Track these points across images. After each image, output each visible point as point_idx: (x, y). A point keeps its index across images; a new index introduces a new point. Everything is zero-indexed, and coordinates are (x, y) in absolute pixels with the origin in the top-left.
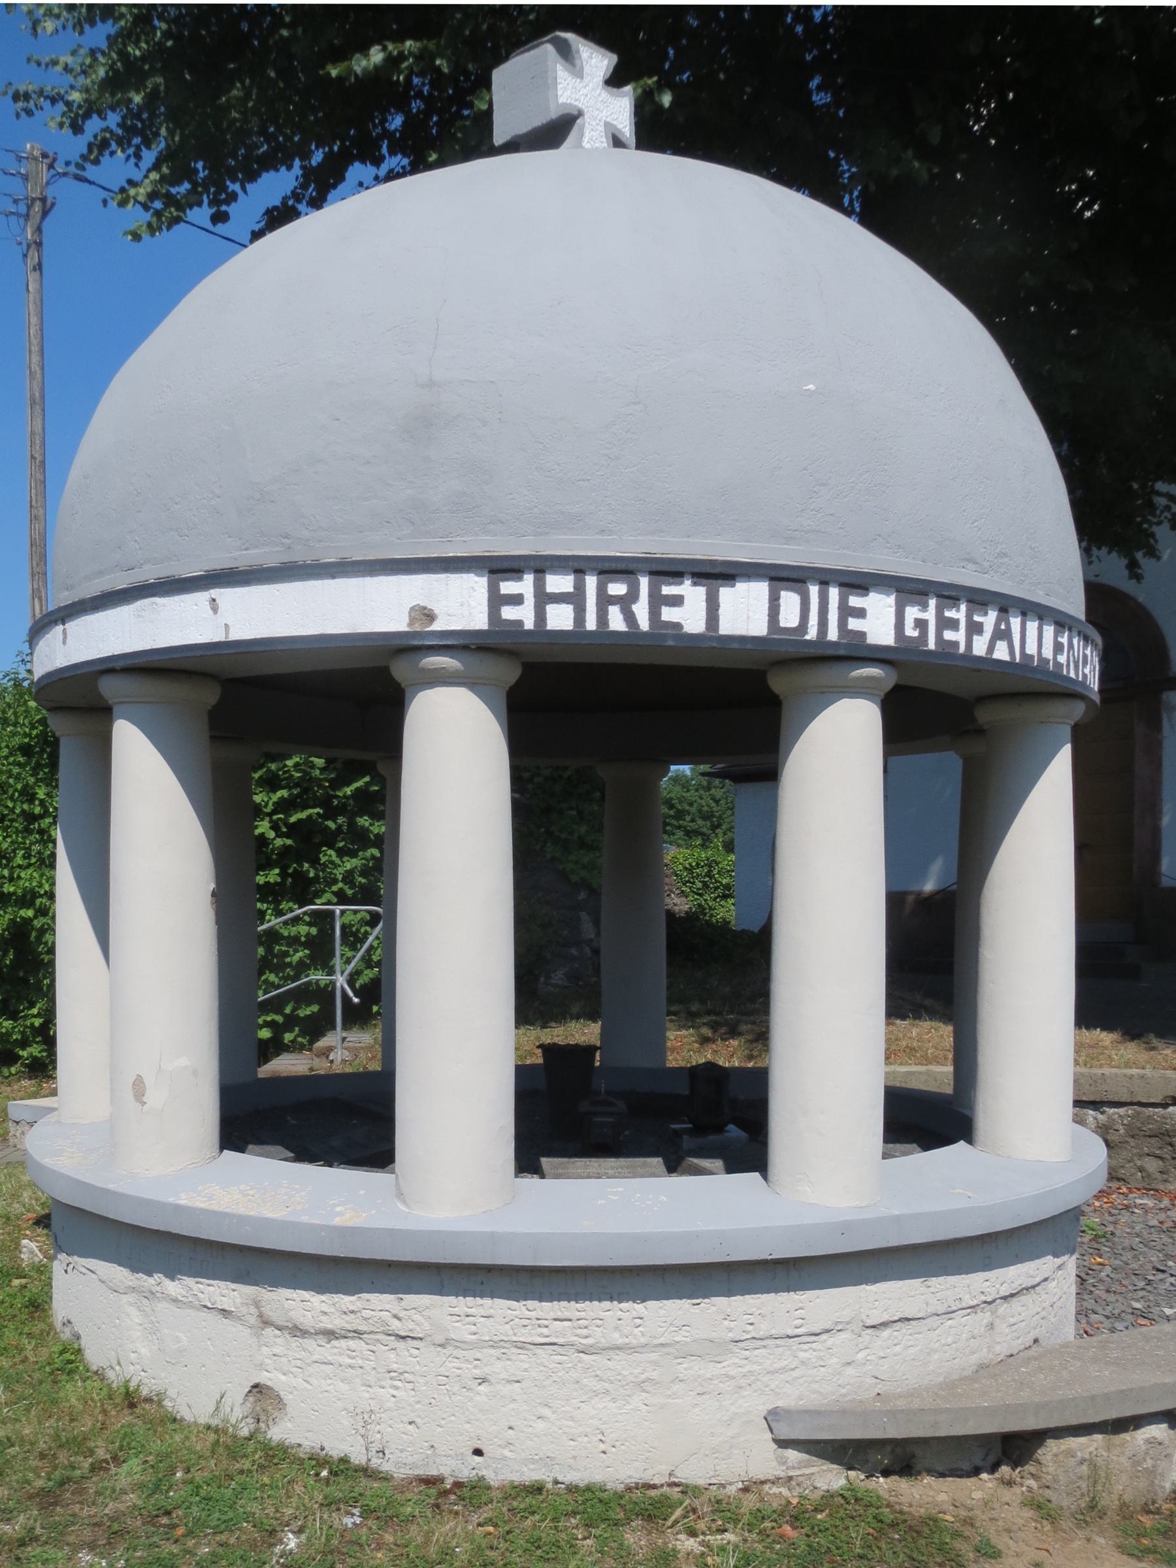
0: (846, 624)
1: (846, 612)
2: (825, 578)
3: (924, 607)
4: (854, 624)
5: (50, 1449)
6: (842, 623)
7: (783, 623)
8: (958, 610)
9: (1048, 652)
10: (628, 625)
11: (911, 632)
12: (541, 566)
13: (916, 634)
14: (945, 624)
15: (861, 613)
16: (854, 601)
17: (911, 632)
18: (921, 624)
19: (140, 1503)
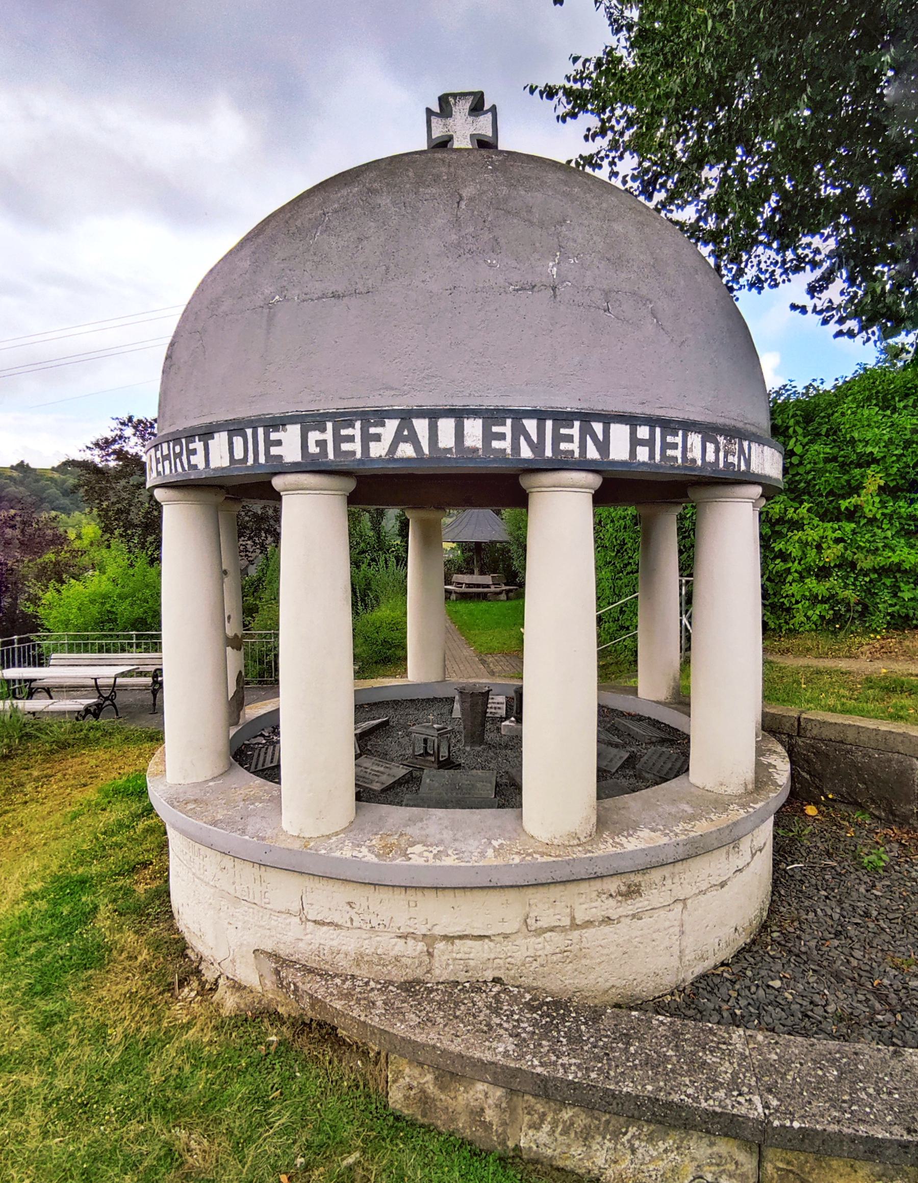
0: (269, 451)
1: (269, 443)
2: (254, 423)
3: (323, 430)
4: (274, 451)
5: (128, 559)
6: (267, 451)
7: (441, 445)
8: (353, 427)
9: (711, 457)
10: (416, 451)
11: (313, 449)
12: (518, 415)
13: (317, 450)
14: (339, 439)
15: (279, 443)
16: (274, 436)
17: (313, 449)
18: (322, 444)
19: (852, 601)
